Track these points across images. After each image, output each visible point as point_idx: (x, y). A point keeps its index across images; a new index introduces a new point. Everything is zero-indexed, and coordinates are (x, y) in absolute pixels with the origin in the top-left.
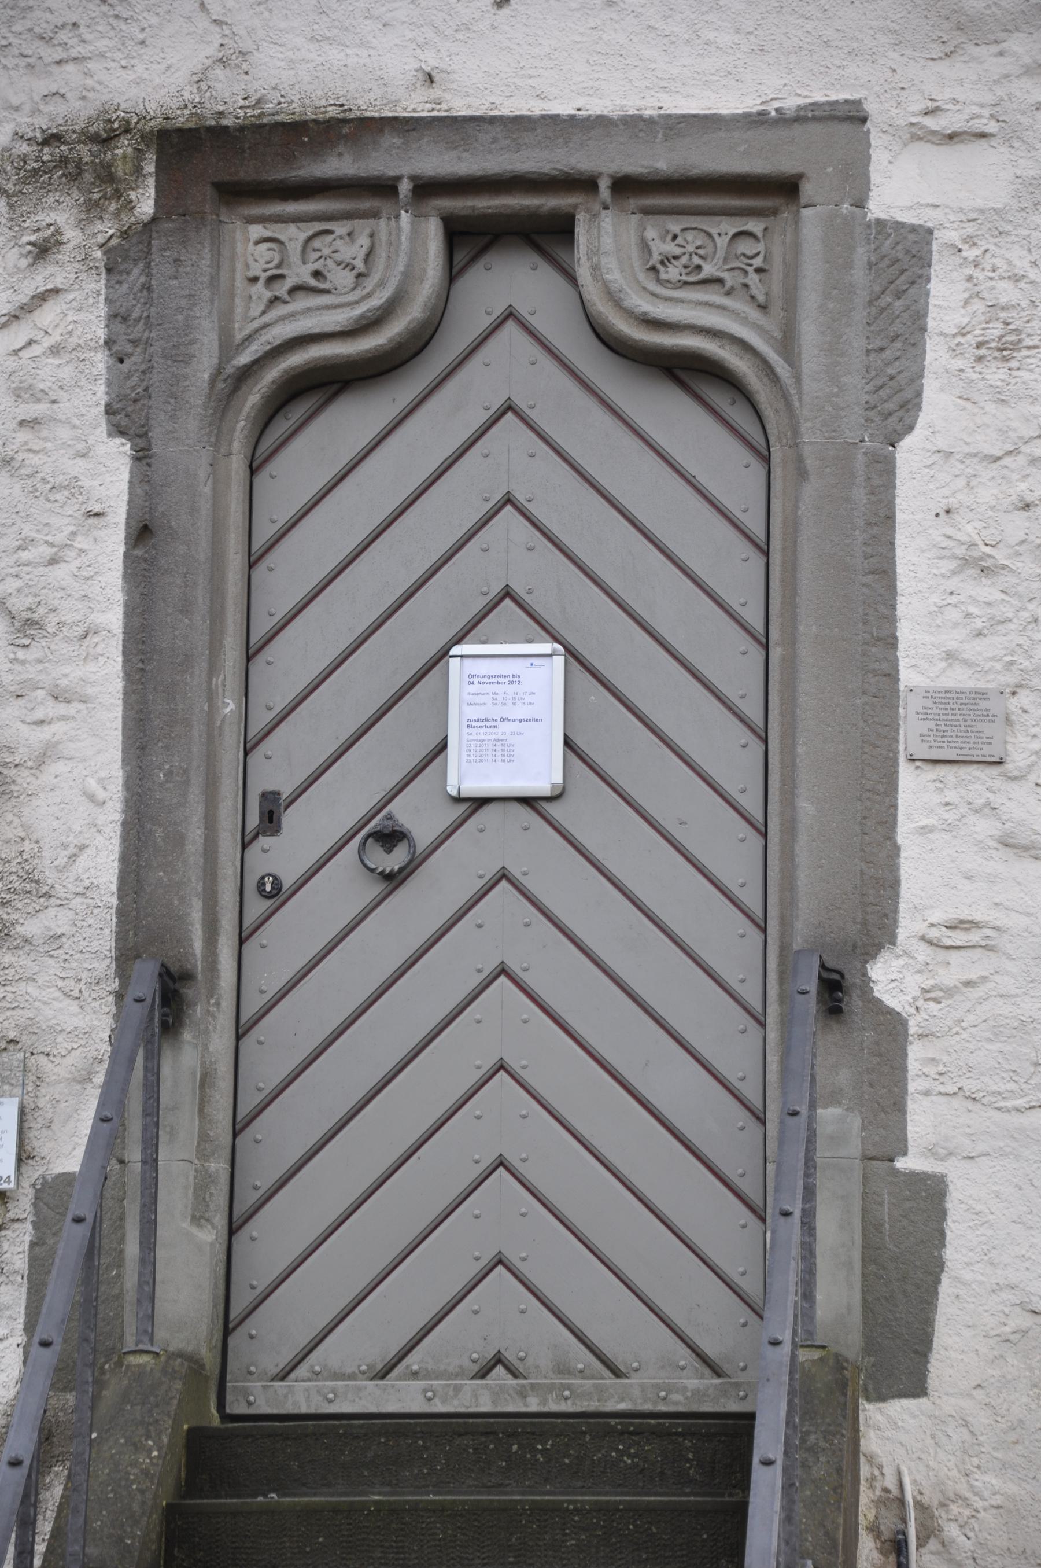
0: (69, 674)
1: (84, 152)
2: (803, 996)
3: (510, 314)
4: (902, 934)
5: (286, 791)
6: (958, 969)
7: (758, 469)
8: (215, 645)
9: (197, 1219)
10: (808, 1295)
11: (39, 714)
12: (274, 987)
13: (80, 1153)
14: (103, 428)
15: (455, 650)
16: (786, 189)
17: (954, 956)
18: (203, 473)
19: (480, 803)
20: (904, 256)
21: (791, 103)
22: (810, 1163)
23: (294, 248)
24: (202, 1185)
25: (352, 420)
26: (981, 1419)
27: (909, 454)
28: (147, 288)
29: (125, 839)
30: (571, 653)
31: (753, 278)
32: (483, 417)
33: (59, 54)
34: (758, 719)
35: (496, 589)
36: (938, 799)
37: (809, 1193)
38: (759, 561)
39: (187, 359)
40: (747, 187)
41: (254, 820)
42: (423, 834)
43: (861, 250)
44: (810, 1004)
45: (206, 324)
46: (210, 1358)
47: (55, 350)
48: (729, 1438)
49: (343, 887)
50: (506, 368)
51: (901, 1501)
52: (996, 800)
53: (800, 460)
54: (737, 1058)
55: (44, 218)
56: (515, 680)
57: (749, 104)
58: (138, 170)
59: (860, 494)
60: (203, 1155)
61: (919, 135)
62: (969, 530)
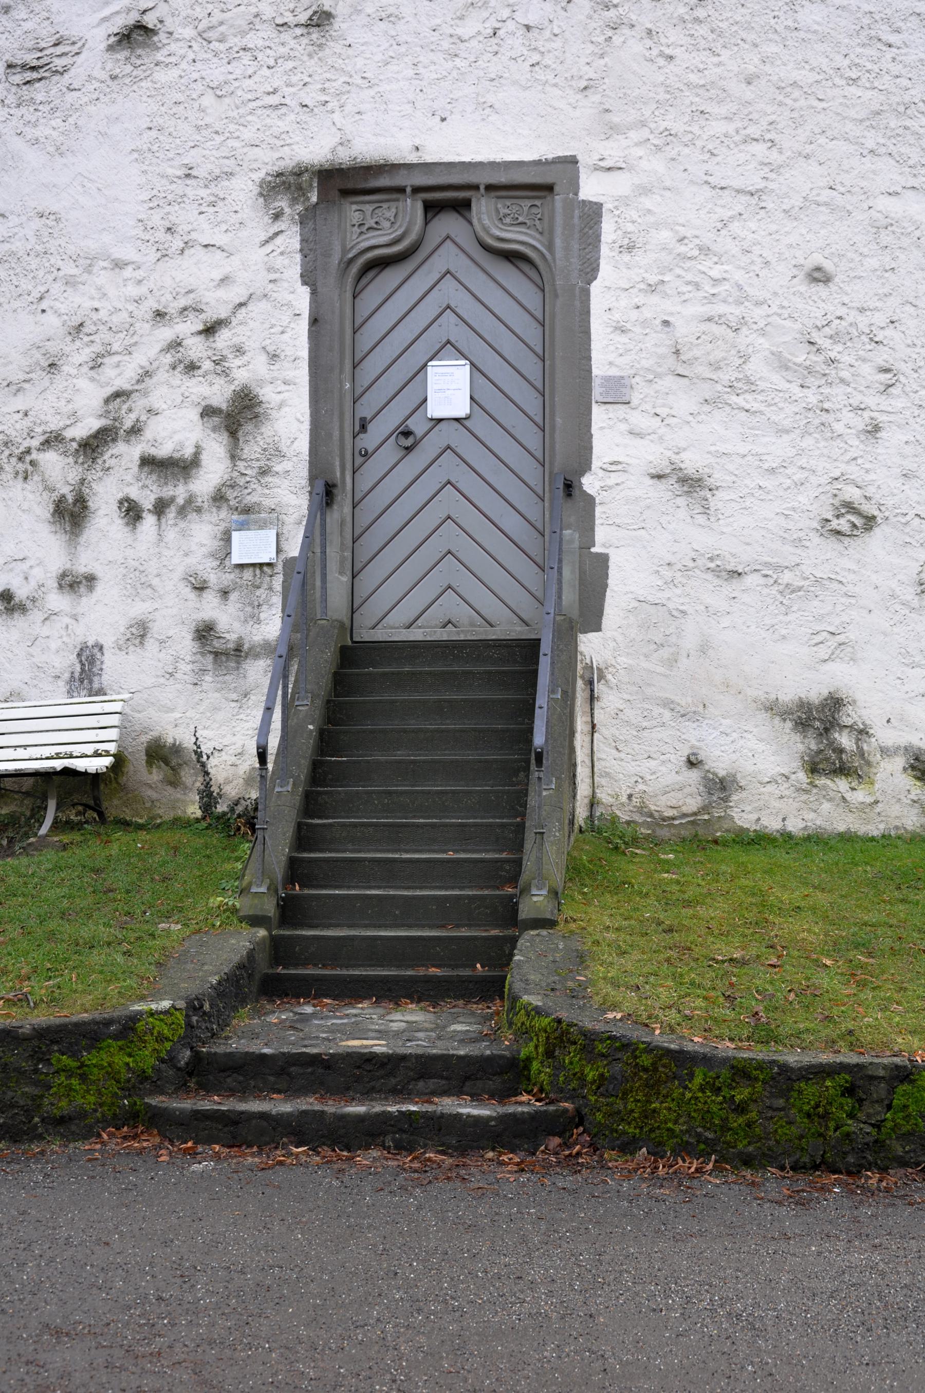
0: (290, 374)
1: (292, 179)
3: (448, 237)
4: (593, 467)
5: (369, 417)
6: (613, 479)
7: (540, 294)
8: (342, 363)
9: (341, 573)
10: (560, 597)
11: (279, 390)
13: (298, 549)
16: (549, 188)
18: (336, 298)
19: (440, 420)
21: (550, 156)
22: (560, 550)
23: (368, 213)
24: (342, 561)
25: (391, 277)
26: (620, 639)
28: (315, 229)
29: (311, 435)
30: (472, 364)
31: (537, 222)
32: (438, 276)
33: (282, 143)
34: (541, 388)
35: (444, 340)
36: (606, 417)
37: (560, 561)
38: (541, 328)
39: (330, 256)
40: (539, 187)
41: (357, 428)
44: (561, 493)
46: (347, 623)
47: (282, 253)
48: (531, 648)
49: (389, 454)
50: (448, 258)
51: (592, 667)
52: (627, 417)
53: (555, 290)
54: (534, 514)
55: (277, 204)
56: (452, 374)
58: (311, 185)
59: (577, 303)
60: (342, 550)
61: (597, 168)
62: (617, 316)
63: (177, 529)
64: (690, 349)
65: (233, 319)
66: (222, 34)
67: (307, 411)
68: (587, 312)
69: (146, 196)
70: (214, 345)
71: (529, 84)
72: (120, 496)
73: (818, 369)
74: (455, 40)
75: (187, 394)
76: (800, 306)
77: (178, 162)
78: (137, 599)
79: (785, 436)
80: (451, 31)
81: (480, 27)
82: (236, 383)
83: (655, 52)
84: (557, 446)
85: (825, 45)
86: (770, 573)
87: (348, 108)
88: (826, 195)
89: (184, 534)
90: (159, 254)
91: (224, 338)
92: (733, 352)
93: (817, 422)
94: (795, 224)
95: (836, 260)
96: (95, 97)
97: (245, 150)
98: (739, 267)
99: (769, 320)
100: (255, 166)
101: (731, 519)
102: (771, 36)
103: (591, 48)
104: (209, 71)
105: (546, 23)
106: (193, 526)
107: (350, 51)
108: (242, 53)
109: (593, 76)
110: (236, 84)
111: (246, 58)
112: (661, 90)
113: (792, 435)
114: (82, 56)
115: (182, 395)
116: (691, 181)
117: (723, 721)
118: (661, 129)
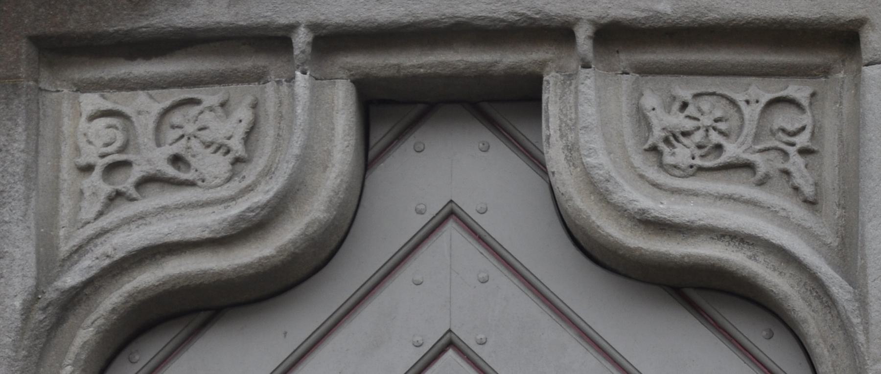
23: (145, 125)
31: (796, 163)
45: (18, 231)
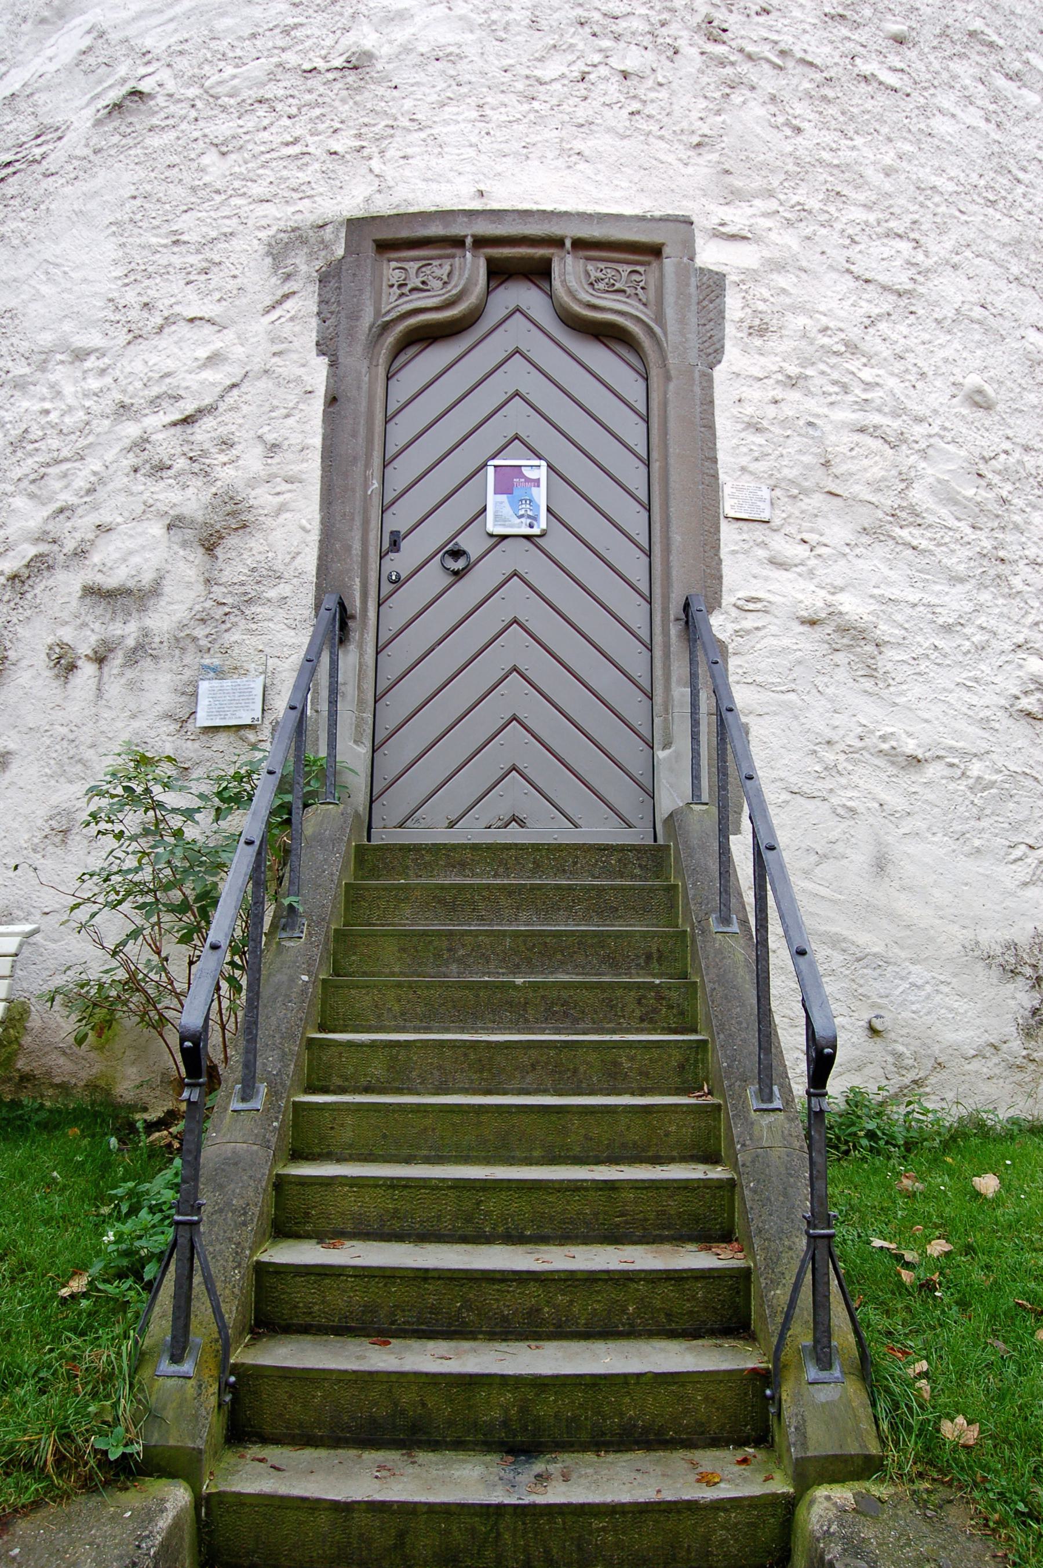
0: (295, 468)
2: (754, 594)
3: (518, 310)
4: (724, 603)
6: (750, 622)
8: (369, 456)
11: (278, 489)
12: (395, 629)
14: (314, 352)
15: (490, 463)
16: (655, 251)
17: (749, 615)
18: (364, 370)
20: (714, 285)
21: (657, 214)
23: (412, 272)
24: (360, 720)
27: (719, 373)
31: (640, 291)
33: (301, 195)
40: (638, 250)
41: (386, 545)
42: (474, 554)
43: (693, 279)
45: (368, 302)
49: (434, 577)
52: (767, 540)
53: (667, 372)
57: (638, 211)
59: (697, 389)
62: (749, 410)
63: (123, 681)
64: (842, 461)
65: (221, 404)
66: (234, 87)
67: (317, 517)
68: (709, 402)
69: (120, 272)
70: (192, 438)
71: (628, 133)
72: (50, 640)
73: (990, 507)
74: (532, 82)
75: (151, 502)
76: (964, 431)
77: (165, 229)
78: (62, 780)
79: (959, 586)
80: (528, 72)
81: (565, 70)
82: (219, 483)
83: (781, 120)
84: (674, 573)
85: (960, 159)
86: (956, 761)
87: (390, 153)
88: (977, 312)
89: (133, 687)
90: (131, 335)
91: (204, 432)
92: (894, 472)
93: (992, 572)
94: (949, 337)
95: (996, 386)
96: (73, 176)
97: (252, 207)
98: (892, 374)
99: (932, 441)
100: (263, 223)
101: (904, 687)
102: (904, 134)
103: (703, 103)
104: (214, 128)
105: (648, 72)
106: (146, 676)
107: (395, 93)
108: (257, 105)
109: (709, 132)
110: (248, 137)
111: (261, 111)
112: (790, 160)
113: (968, 586)
114: (64, 140)
115: (145, 503)
116: (830, 266)
117: (912, 968)
118: (793, 202)
